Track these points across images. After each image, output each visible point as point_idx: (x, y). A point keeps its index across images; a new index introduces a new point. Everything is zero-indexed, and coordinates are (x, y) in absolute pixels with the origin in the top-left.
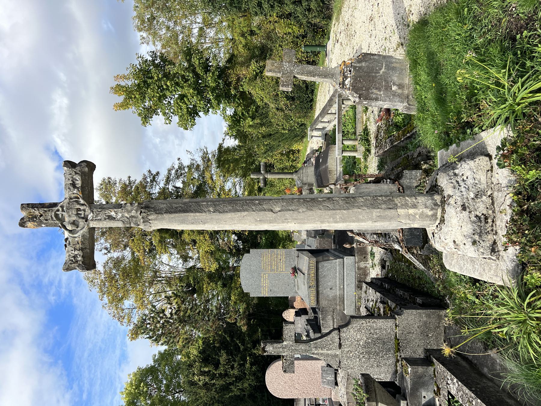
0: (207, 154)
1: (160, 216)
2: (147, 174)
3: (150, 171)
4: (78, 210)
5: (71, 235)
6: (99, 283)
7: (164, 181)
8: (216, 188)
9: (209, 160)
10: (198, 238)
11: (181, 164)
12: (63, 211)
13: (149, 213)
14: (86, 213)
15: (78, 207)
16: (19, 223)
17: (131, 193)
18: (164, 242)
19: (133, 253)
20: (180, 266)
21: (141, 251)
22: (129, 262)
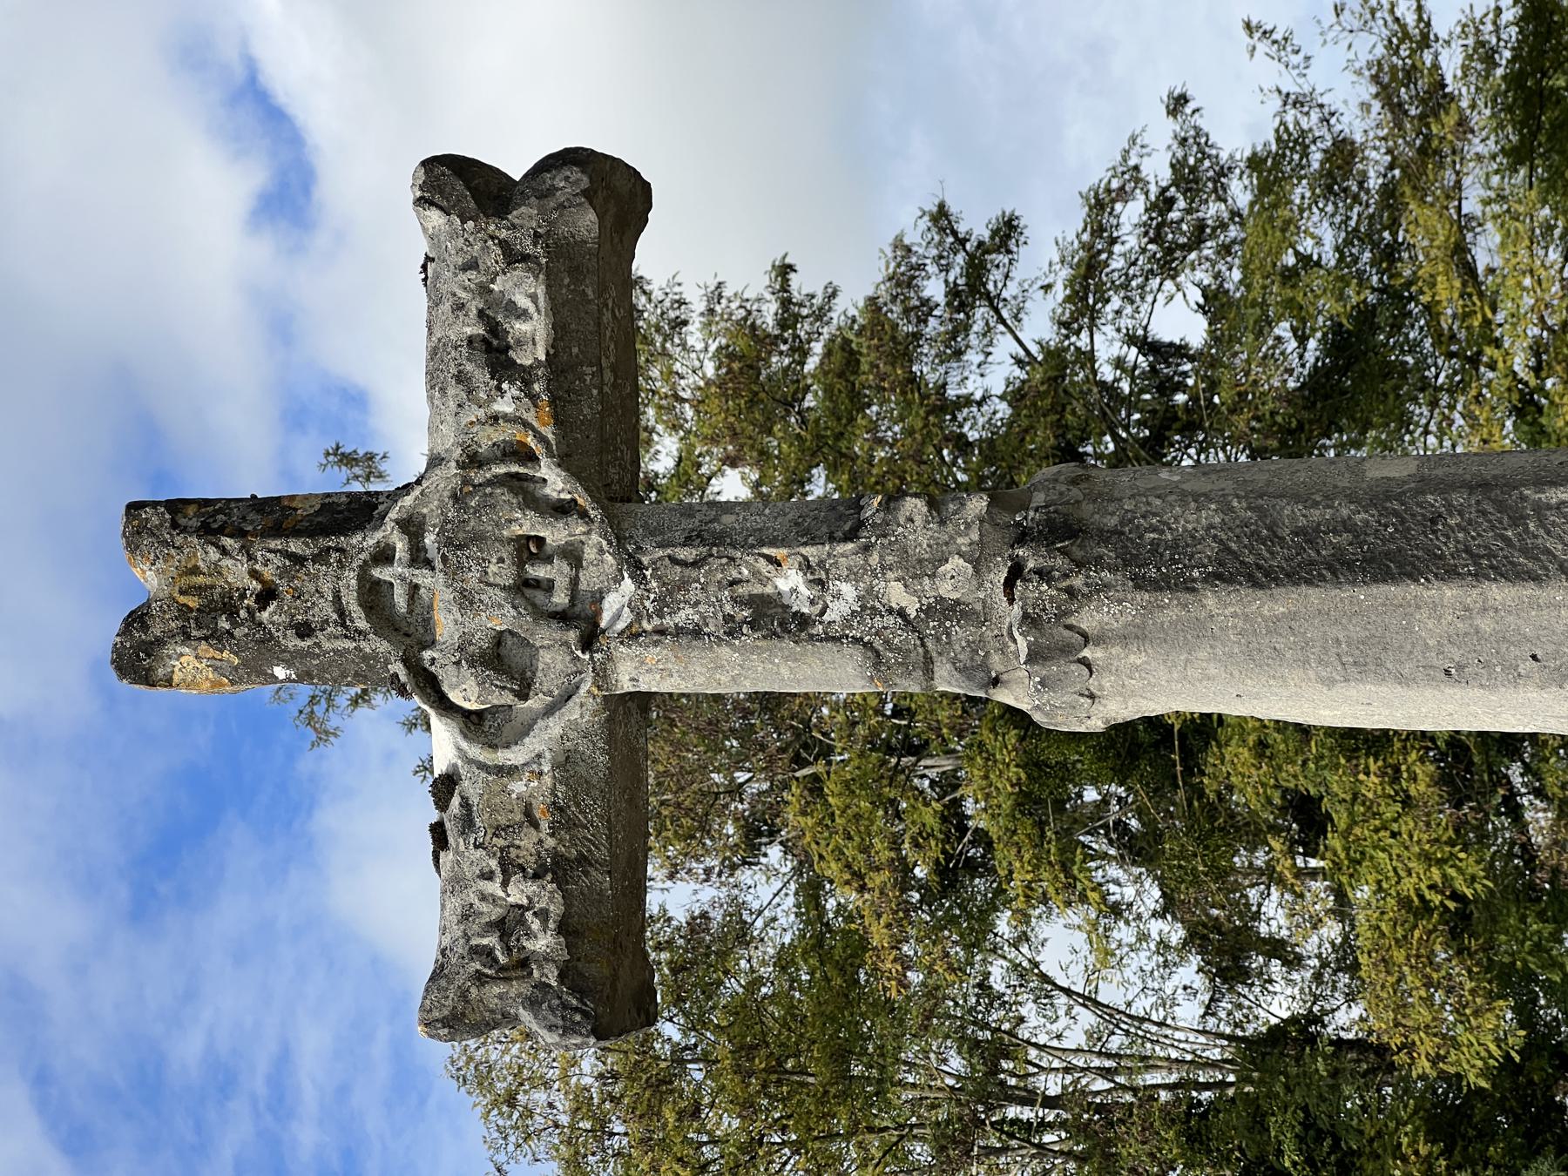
0: (1425, 41)
1: (1171, 609)
2: (917, 234)
3: (941, 217)
4: (529, 549)
5: (475, 751)
6: (564, 1119)
7: (1060, 292)
8: (1497, 343)
9: (1437, 97)
10: (1337, 783)
11: (1194, 141)
12: (418, 558)
13: (1078, 582)
14: (589, 579)
15: (526, 529)
16: (118, 651)
17: (791, 402)
18: (1059, 806)
19: (812, 893)
20: (1189, 1012)
21: (878, 879)
22: (784, 960)
